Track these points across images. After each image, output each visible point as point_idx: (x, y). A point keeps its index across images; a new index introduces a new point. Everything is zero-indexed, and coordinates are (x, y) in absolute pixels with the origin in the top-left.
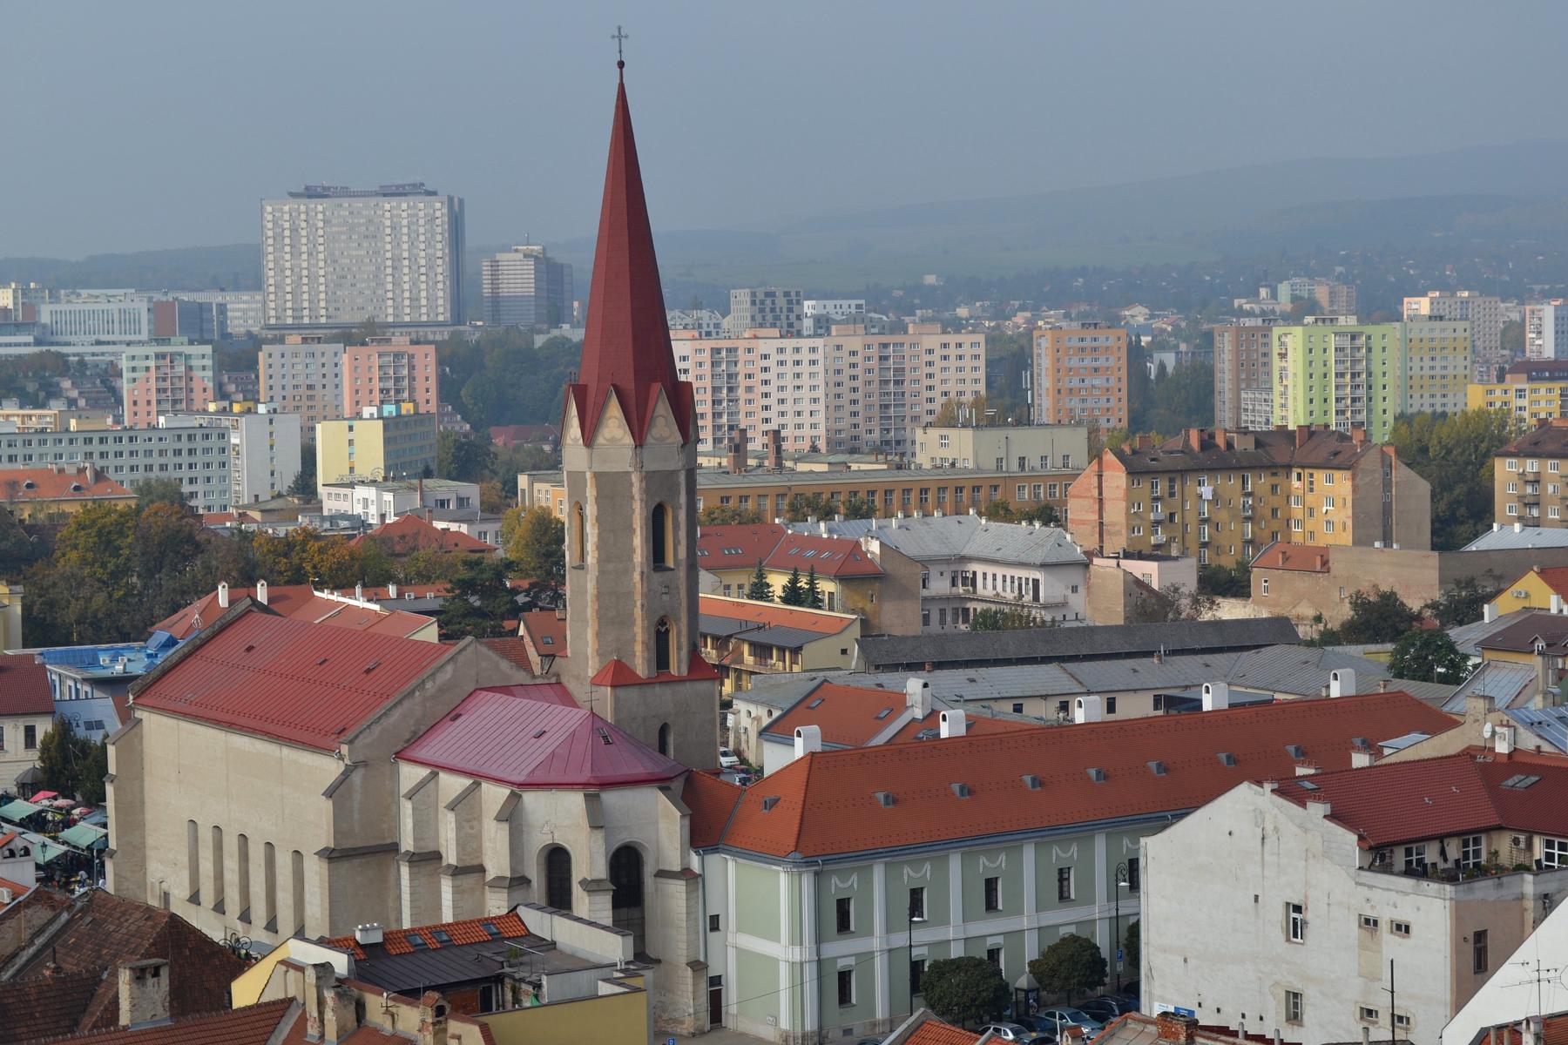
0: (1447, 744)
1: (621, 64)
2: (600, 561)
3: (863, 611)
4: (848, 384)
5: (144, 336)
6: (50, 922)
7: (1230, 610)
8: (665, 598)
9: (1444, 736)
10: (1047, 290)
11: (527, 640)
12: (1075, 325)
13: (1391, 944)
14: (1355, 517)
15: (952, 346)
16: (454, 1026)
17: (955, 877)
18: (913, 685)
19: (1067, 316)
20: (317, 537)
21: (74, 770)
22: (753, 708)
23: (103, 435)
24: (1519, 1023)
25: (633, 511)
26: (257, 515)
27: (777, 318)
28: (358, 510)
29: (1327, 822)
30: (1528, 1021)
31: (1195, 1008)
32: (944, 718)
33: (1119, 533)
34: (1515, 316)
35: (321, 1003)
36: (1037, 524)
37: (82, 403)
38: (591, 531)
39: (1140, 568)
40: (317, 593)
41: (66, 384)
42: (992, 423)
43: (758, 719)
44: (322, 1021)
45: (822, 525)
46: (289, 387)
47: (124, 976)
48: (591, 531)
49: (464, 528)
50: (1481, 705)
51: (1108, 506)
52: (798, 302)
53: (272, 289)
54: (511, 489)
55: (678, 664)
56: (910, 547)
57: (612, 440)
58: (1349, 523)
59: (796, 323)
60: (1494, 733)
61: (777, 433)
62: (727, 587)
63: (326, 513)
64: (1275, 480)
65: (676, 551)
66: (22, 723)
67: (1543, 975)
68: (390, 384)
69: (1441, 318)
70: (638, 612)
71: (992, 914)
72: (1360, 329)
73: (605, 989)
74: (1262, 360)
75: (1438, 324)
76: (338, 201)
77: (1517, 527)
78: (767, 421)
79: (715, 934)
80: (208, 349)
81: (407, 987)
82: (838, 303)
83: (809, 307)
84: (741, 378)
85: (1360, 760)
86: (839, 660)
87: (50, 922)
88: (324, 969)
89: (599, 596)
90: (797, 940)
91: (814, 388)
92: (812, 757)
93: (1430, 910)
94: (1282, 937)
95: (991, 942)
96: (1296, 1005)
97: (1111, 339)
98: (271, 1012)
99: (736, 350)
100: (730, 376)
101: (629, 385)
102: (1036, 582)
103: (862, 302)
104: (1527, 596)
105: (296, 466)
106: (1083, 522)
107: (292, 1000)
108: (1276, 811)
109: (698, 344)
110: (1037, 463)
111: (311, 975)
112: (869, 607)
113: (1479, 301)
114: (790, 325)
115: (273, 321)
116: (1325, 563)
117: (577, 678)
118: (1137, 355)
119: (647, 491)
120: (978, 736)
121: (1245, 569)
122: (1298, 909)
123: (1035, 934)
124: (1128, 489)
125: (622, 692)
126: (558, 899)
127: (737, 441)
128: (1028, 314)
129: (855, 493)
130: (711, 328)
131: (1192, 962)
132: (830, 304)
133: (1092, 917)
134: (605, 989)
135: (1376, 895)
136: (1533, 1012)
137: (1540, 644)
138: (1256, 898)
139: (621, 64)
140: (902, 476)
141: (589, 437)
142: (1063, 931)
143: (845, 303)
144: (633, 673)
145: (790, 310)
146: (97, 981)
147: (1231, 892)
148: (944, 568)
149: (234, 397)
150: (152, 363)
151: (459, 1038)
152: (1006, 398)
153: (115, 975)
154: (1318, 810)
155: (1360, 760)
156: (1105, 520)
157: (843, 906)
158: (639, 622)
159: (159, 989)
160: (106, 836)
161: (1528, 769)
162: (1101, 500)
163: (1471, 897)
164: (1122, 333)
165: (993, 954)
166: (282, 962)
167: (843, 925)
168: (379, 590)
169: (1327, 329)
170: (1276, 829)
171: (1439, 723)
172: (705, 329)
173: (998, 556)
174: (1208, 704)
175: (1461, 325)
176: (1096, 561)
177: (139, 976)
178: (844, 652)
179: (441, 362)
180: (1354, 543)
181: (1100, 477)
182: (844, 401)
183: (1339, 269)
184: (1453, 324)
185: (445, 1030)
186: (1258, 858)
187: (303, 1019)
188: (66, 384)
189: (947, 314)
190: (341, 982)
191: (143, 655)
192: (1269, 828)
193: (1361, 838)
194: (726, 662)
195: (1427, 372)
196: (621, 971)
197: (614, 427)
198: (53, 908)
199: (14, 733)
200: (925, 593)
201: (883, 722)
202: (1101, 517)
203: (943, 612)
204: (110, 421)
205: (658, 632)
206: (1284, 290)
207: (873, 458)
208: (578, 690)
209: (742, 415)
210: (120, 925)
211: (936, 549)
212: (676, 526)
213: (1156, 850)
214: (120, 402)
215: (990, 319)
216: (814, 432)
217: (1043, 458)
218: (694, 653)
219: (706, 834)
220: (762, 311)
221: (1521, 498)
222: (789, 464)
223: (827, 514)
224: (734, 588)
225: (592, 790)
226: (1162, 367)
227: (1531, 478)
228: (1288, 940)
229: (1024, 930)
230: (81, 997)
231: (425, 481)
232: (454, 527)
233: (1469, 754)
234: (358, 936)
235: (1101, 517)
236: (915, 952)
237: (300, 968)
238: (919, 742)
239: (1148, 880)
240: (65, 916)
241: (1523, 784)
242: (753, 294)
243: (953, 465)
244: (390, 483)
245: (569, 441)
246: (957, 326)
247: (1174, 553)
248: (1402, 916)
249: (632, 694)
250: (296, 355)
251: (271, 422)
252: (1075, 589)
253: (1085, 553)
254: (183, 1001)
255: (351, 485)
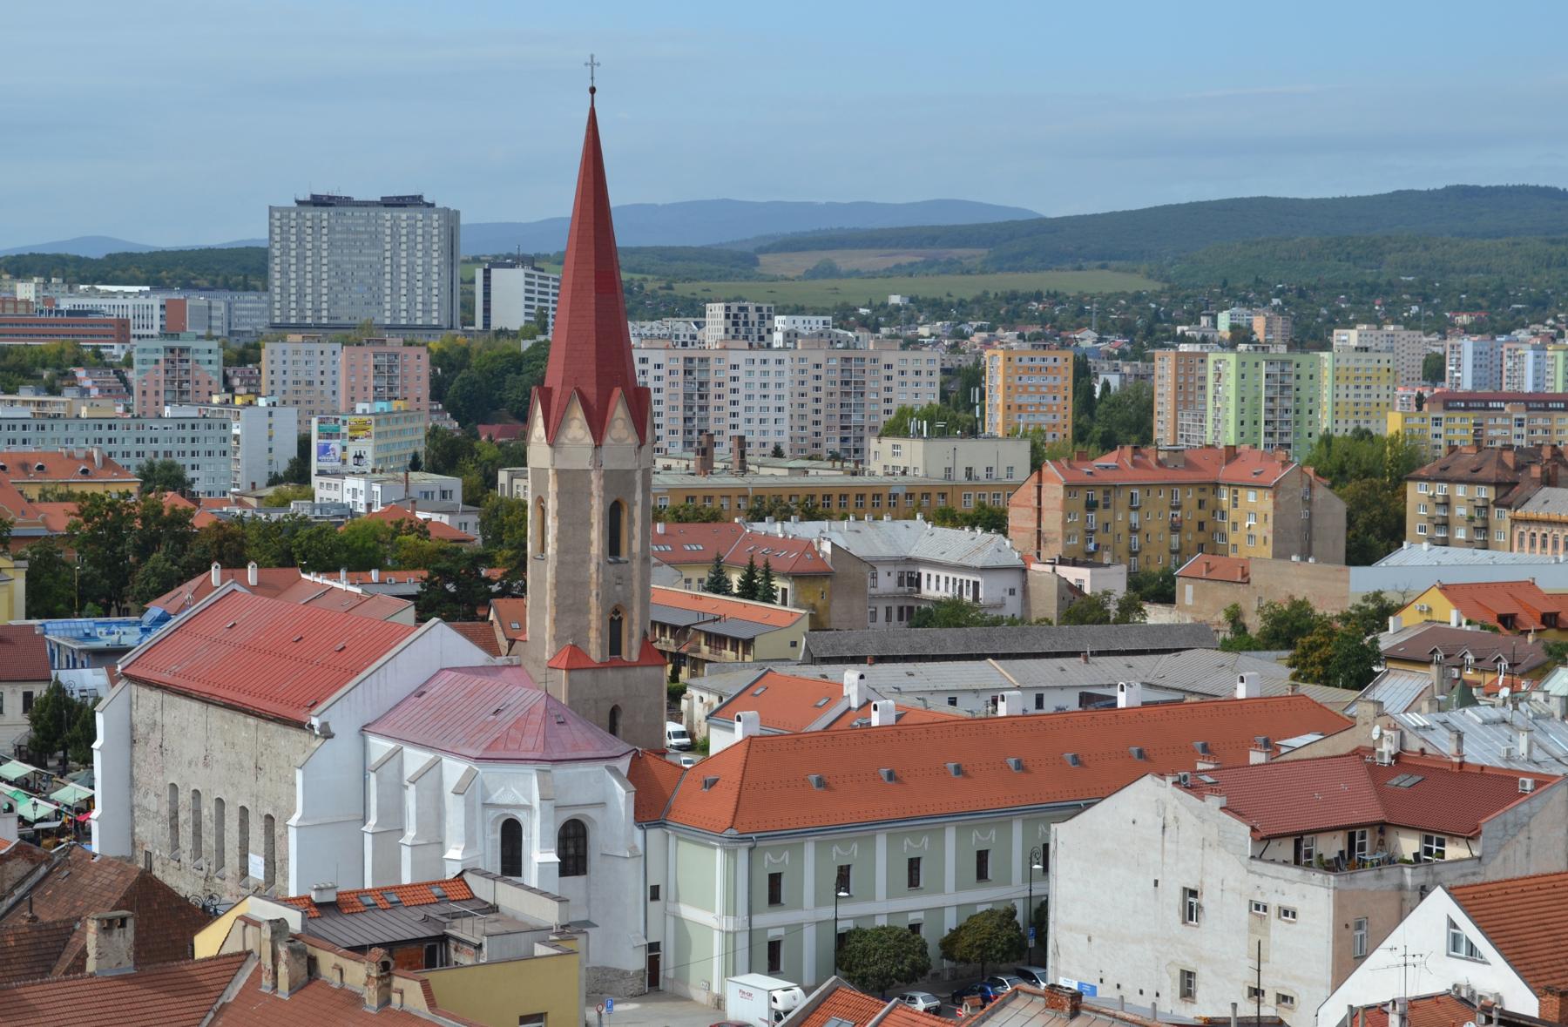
0: (1343, 743)
1: (593, 90)
2: (559, 552)
3: (813, 607)
4: (812, 395)
5: (156, 331)
6: (30, 874)
7: (1157, 615)
8: (619, 588)
9: (1336, 737)
10: (1006, 312)
11: (497, 624)
12: (1027, 346)
13: (1277, 925)
14: (1275, 532)
15: (772, 362)
16: (398, 982)
17: (880, 860)
18: (850, 677)
19: (1021, 337)
20: (309, 524)
21: (60, 735)
22: (705, 696)
23: (112, 422)
24: (1386, 1004)
25: (591, 507)
26: (253, 502)
27: (749, 331)
28: (348, 499)
29: (1222, 814)
30: (1394, 1002)
31: (1097, 983)
32: (875, 708)
33: (1055, 540)
34: (1439, 350)
35: (275, 956)
36: (979, 531)
37: (95, 392)
38: (552, 524)
39: (1072, 574)
40: (304, 576)
41: (81, 373)
42: (943, 434)
43: (710, 705)
44: (275, 973)
45: (779, 525)
46: (289, 383)
47: (93, 926)
48: (552, 524)
49: (445, 519)
50: (1371, 709)
51: (1045, 515)
52: (769, 318)
53: (278, 290)
54: (491, 482)
55: (631, 649)
56: (859, 549)
57: (620, 441)
58: (1270, 538)
59: (767, 337)
60: (1382, 734)
61: (742, 438)
62: (688, 581)
63: (317, 501)
64: (1203, 496)
65: (634, 542)
66: (21, 689)
67: (1410, 960)
68: (384, 382)
69: (1366, 349)
70: (593, 600)
71: (776, 908)
72: (1290, 357)
73: (540, 950)
74: (1198, 383)
75: (1364, 355)
76: (341, 209)
77: (1425, 545)
78: (734, 427)
79: (655, 903)
80: (214, 345)
81: (355, 944)
82: (807, 318)
83: (780, 322)
84: (711, 386)
85: (1257, 757)
86: (788, 652)
87: (30, 874)
88: (279, 926)
89: (558, 584)
90: (731, 909)
91: (780, 397)
92: (750, 740)
93: (1314, 898)
94: (1179, 919)
95: (913, 918)
96: (1189, 983)
97: (1063, 363)
98: (231, 963)
99: (707, 360)
100: (701, 384)
101: (591, 391)
102: (976, 584)
103: (829, 318)
104: (1430, 610)
105: (293, 453)
106: (1023, 530)
107: (248, 953)
108: (1176, 802)
109: (672, 353)
110: (1003, 474)
111: (267, 933)
112: (819, 603)
113: (1405, 334)
114: (761, 338)
115: (277, 320)
116: (1244, 575)
117: (535, 661)
118: (1082, 372)
119: (605, 489)
120: (901, 724)
121: (1170, 579)
122: (1194, 893)
123: (813, 928)
124: (1065, 500)
125: (576, 675)
126: (512, 863)
127: (704, 445)
128: (985, 335)
129: (693, 498)
130: (687, 339)
131: (1096, 941)
132: (799, 319)
133: (1008, 891)
134: (540, 950)
135: (1266, 883)
136: (1397, 993)
137: (1440, 656)
138: (1156, 882)
139: (593, 90)
140: (858, 480)
141: (553, 437)
142: (980, 909)
143: (813, 319)
144: (588, 657)
145: (762, 323)
146: (70, 930)
147: (1130, 878)
148: (890, 568)
149: (238, 391)
150: (161, 357)
151: (401, 993)
152: (957, 408)
153: (84, 926)
154: (1214, 802)
155: (1257, 757)
156: (1043, 528)
157: (775, 880)
158: (594, 610)
159: (124, 940)
160: (92, 798)
161: (1413, 769)
162: (1039, 510)
163: (1353, 886)
164: (1070, 354)
165: (915, 928)
166: (242, 918)
167: (775, 898)
168: (363, 574)
169: (1260, 354)
170: (1176, 819)
171: (1334, 724)
172: (682, 339)
173: (942, 558)
174: (1122, 701)
175: (1384, 357)
176: (1034, 567)
177: (108, 926)
178: (794, 644)
179: (433, 364)
180: (1274, 557)
181: (1039, 488)
182: (808, 410)
183: (1275, 301)
184: (1378, 356)
185: (389, 985)
186: (1159, 846)
187: (258, 971)
188: (81, 373)
189: (909, 333)
190: (295, 938)
191: (137, 629)
192: (1170, 818)
193: (1253, 829)
194: (683, 650)
195: (1352, 399)
196: (557, 934)
197: (577, 429)
198: (32, 861)
199: (13, 699)
200: (873, 591)
201: (820, 710)
202: (1039, 525)
203: (888, 610)
204: (120, 409)
205: (612, 620)
206: (1224, 320)
207: (830, 464)
208: (539, 674)
209: (711, 421)
210: (94, 879)
211: (885, 551)
212: (631, 521)
213: (1064, 835)
214: (130, 391)
215: (949, 338)
216: (778, 439)
217: (989, 469)
218: (646, 643)
219: (651, 809)
220: (735, 324)
221: (1431, 519)
222: (752, 468)
223: (784, 516)
224: (695, 582)
225: (547, 766)
226: (1106, 386)
227: (1440, 500)
228: (1184, 922)
229: (948, 902)
230: (50, 950)
231: (411, 474)
232: (436, 517)
233: (1359, 753)
234: (314, 896)
235: (1039, 525)
236: (840, 925)
237: (257, 924)
238: (850, 733)
239: (1058, 863)
240: (43, 869)
241: (1407, 784)
242: (728, 308)
243: (904, 473)
244: (377, 475)
245: (533, 439)
246: (912, 343)
247: (1107, 560)
248: (1288, 903)
249: (586, 676)
250: (296, 352)
251: (270, 414)
252: (1012, 592)
253: (1022, 558)
254: (144, 952)
255: (342, 476)
